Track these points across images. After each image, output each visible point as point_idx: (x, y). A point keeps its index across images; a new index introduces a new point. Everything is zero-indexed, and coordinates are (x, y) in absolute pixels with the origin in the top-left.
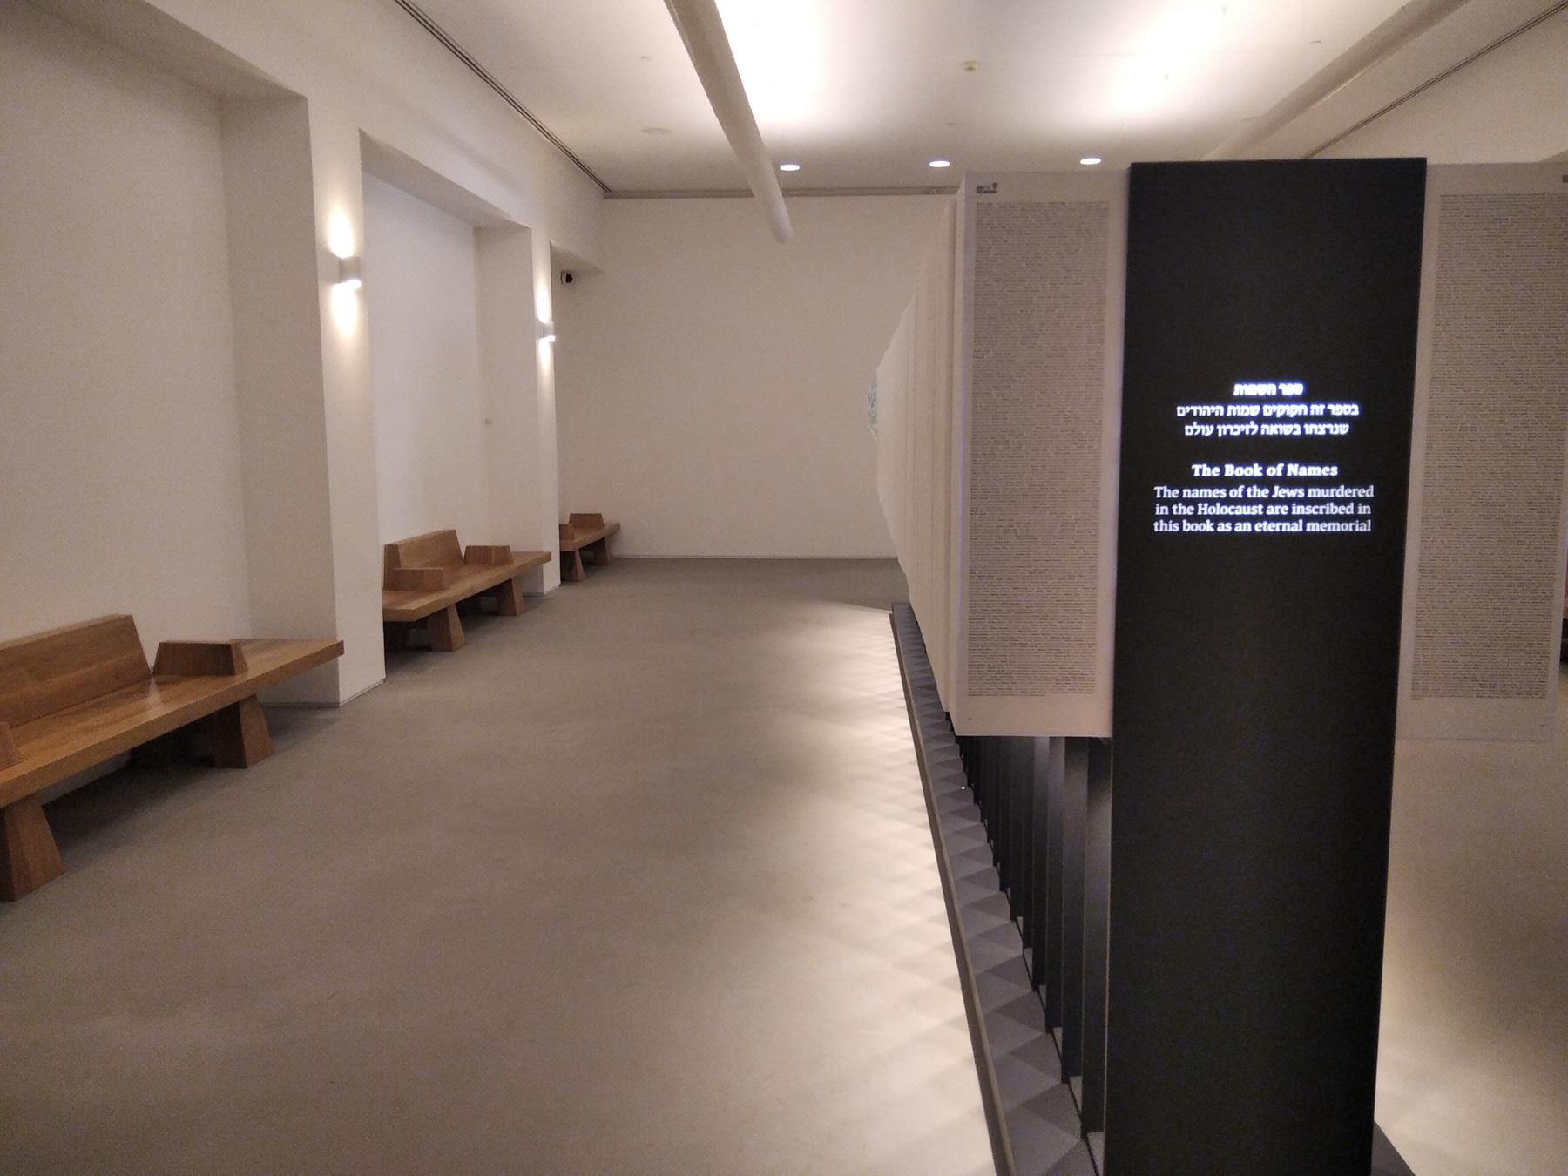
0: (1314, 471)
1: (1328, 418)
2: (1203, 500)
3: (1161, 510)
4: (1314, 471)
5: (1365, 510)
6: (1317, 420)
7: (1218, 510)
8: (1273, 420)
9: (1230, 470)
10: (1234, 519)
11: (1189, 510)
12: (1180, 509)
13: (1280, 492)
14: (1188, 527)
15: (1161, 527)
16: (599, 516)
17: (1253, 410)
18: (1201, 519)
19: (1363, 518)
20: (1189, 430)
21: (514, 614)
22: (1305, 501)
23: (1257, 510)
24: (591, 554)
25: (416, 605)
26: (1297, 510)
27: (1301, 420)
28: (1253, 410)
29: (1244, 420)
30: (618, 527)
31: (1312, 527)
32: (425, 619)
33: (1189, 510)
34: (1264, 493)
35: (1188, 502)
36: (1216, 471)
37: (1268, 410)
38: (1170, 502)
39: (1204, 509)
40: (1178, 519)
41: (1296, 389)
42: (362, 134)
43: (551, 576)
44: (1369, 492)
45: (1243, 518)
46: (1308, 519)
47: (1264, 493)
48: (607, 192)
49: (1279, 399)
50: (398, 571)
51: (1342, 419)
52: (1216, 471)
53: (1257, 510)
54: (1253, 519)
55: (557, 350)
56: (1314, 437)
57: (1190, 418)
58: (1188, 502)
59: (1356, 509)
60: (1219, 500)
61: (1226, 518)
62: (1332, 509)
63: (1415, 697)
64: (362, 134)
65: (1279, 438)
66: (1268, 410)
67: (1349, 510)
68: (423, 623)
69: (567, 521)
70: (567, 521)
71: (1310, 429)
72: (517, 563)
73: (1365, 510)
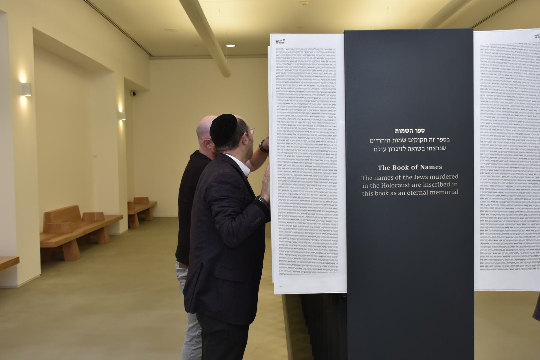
0: (432, 167)
1: (436, 143)
2: (384, 181)
3: (365, 186)
4: (432, 167)
5: (455, 185)
6: (432, 144)
7: (390, 186)
8: (413, 144)
9: (395, 168)
10: (398, 190)
11: (377, 186)
12: (374, 186)
13: (417, 177)
14: (377, 194)
15: (365, 194)
16: (147, 198)
17: (404, 140)
18: (384, 190)
19: (455, 189)
20: (375, 150)
21: (105, 244)
22: (429, 181)
23: (408, 185)
24: (142, 216)
25: (56, 241)
26: (425, 185)
27: (425, 144)
28: (404, 140)
29: (400, 145)
30: (155, 204)
31: (432, 193)
32: (62, 245)
33: (377, 186)
34: (410, 178)
35: (377, 182)
36: (388, 168)
37: (410, 140)
38: (369, 183)
39: (384, 185)
40: (373, 190)
41: (422, 130)
42: (35, 31)
43: (123, 226)
44: (457, 177)
45: (402, 189)
46: (430, 189)
47: (410, 178)
48: (151, 55)
49: (415, 135)
50: (51, 223)
51: (443, 144)
52: (388, 168)
53: (408, 185)
54: (406, 190)
55: (125, 123)
56: (431, 151)
57: (376, 144)
58: (377, 182)
59: (451, 185)
60: (390, 181)
61: (393, 190)
62: (441, 185)
63: (482, 270)
64: (35, 31)
65: (416, 152)
66: (410, 140)
67: (448, 185)
68: (61, 247)
69: (132, 200)
70: (132, 200)
71: (429, 148)
72: (107, 220)
73: (455, 185)
